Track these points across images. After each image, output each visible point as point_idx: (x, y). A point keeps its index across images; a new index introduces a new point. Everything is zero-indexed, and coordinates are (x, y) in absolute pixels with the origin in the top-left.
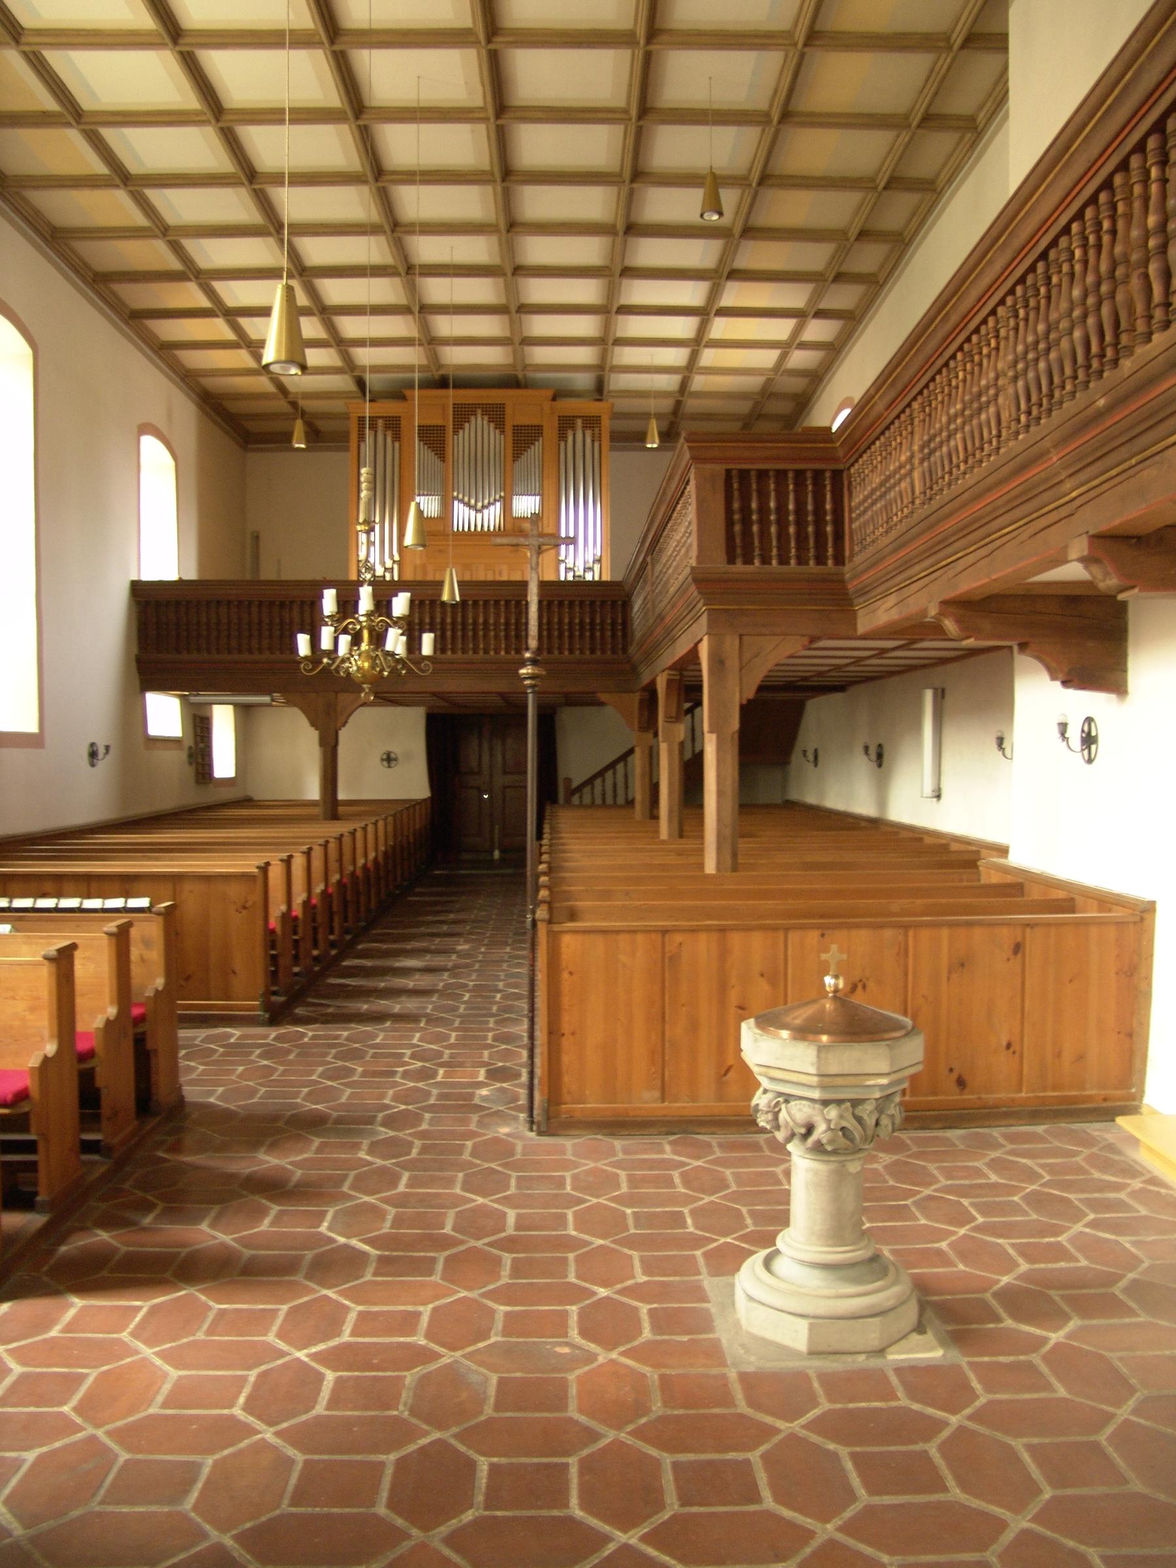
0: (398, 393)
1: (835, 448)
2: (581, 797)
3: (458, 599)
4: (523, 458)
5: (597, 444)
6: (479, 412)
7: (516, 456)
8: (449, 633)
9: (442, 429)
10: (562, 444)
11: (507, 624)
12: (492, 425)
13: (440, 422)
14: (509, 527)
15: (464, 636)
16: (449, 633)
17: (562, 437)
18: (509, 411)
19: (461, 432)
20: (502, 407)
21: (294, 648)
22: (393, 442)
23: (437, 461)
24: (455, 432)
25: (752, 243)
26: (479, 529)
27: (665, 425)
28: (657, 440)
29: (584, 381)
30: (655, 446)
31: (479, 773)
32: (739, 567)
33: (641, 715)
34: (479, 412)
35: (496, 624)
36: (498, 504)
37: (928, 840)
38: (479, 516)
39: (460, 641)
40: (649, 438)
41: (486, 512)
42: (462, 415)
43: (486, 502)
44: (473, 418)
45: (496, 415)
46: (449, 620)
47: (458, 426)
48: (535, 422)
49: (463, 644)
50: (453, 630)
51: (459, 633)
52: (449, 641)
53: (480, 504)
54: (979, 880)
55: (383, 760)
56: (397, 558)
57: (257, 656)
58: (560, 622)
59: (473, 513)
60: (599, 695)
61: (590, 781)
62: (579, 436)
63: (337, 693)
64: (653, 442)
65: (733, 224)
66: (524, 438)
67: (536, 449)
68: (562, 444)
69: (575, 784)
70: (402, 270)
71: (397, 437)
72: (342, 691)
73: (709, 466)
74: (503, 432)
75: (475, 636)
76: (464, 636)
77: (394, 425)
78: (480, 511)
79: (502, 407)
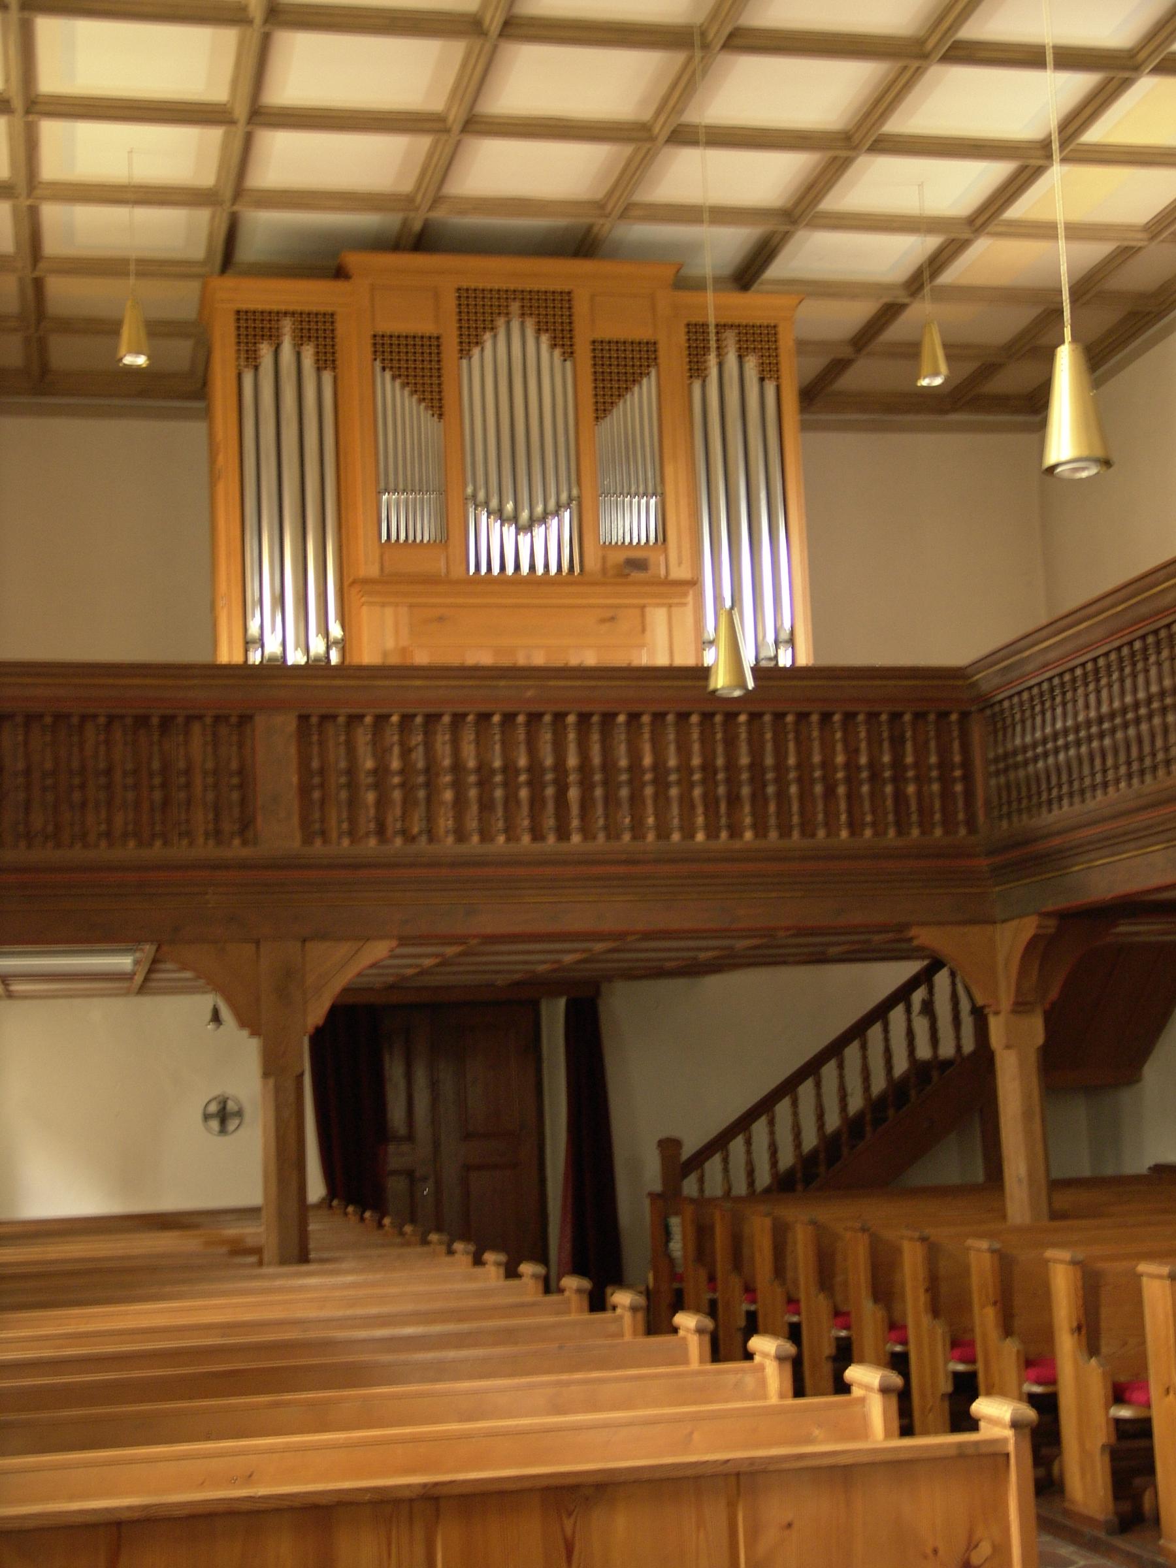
2: (701, 1180)
3: (751, 684)
4: (618, 412)
5: (770, 388)
6: (515, 307)
8: (573, 794)
9: (434, 343)
10: (697, 386)
11: (708, 768)
12: (545, 339)
13: (426, 327)
14: (592, 563)
15: (610, 800)
16: (573, 794)
17: (696, 369)
18: (581, 308)
19: (476, 351)
20: (565, 299)
22: (319, 370)
23: (427, 420)
24: (464, 352)
26: (525, 569)
27: (816, 364)
28: (943, 368)
31: (410, 1138)
33: (1023, 972)
35: (685, 768)
36: (567, 515)
38: (524, 540)
39: (600, 810)
40: (926, 364)
41: (539, 531)
43: (539, 509)
44: (501, 322)
47: (469, 340)
51: (599, 792)
52: (575, 810)
53: (525, 515)
55: (207, 1117)
56: (336, 631)
57: (103, 853)
59: (510, 531)
61: (720, 1143)
64: (936, 374)
65: (449, 109)
67: (645, 393)
68: (697, 386)
70: (18, 103)
71: (327, 360)
72: (322, 936)
74: (569, 354)
75: (636, 799)
76: (610, 800)
78: (529, 528)
79: (565, 299)
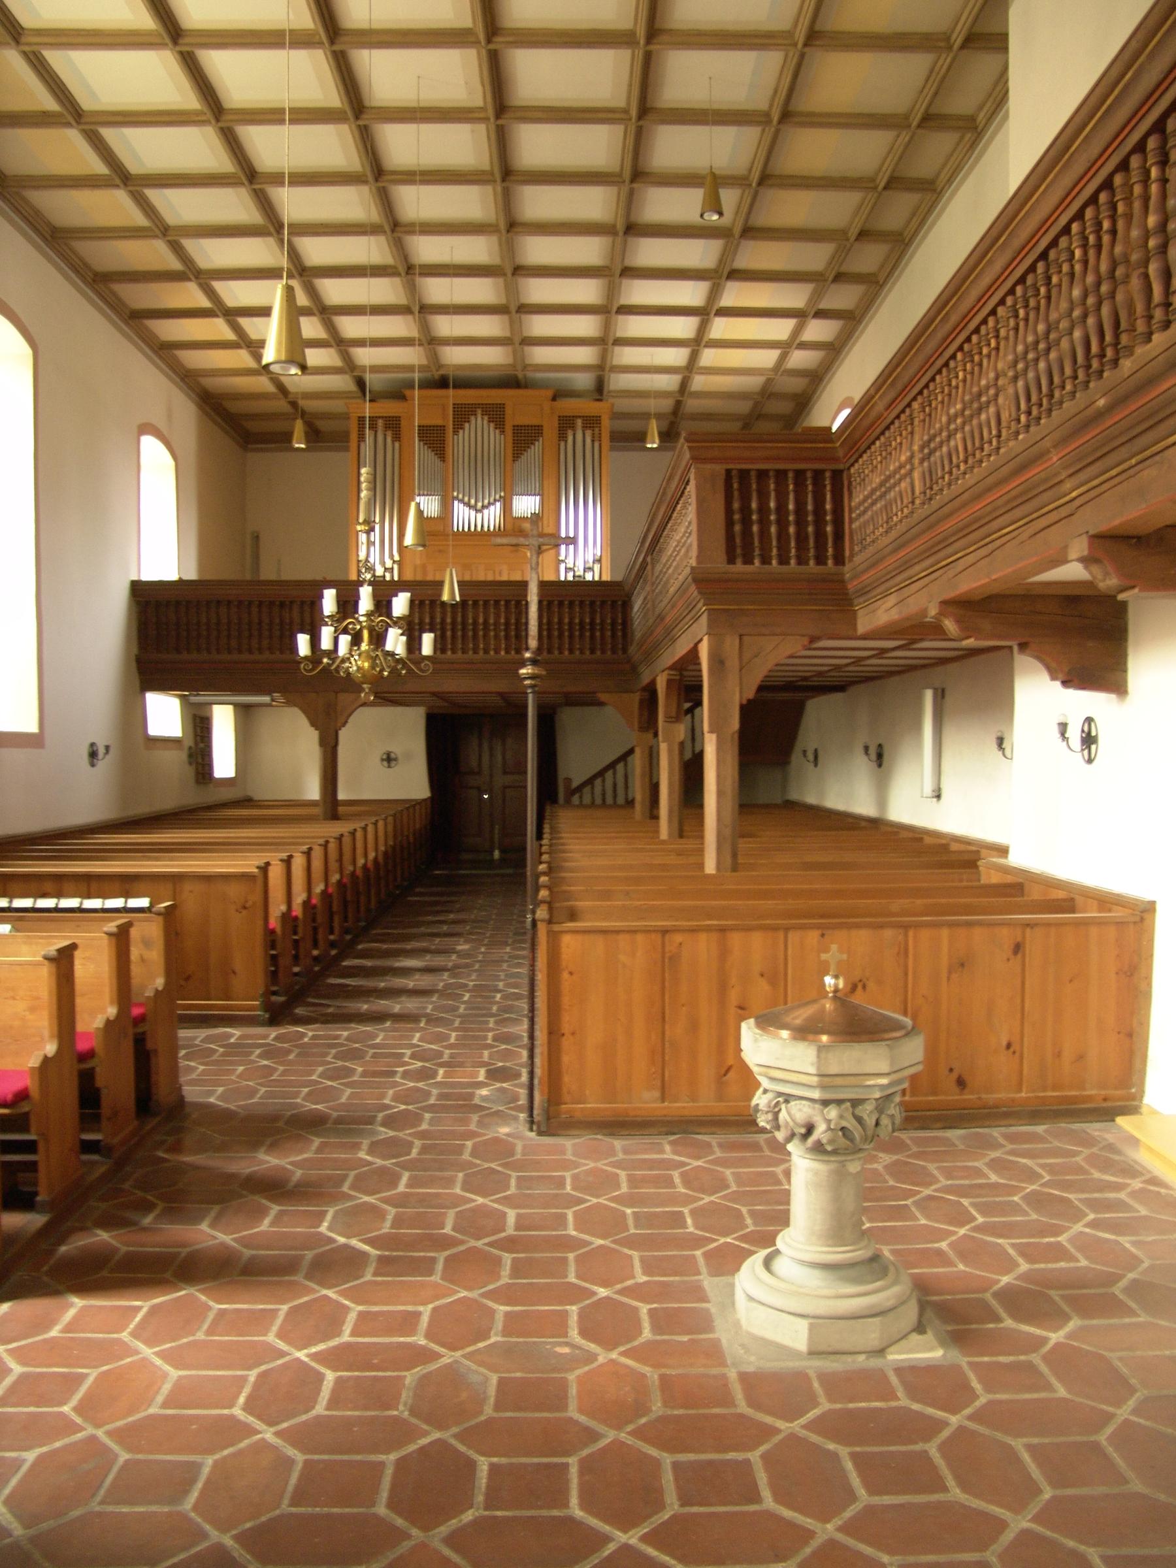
0: (398, 393)
1: (835, 448)
2: (581, 797)
3: (458, 599)
4: (523, 458)
5: (597, 444)
6: (479, 412)
7: (516, 456)
8: (449, 633)
9: (442, 429)
10: (562, 444)
11: (507, 624)
12: (492, 425)
13: (440, 422)
14: (509, 527)
15: (464, 636)
16: (449, 633)
17: (562, 437)
18: (509, 411)
19: (461, 432)
20: (502, 407)
21: (294, 648)
22: (393, 442)
23: (437, 461)
24: (455, 432)
25: (752, 243)
26: (479, 529)
27: (665, 425)
28: (657, 440)
29: (584, 381)
30: (655, 446)
31: (479, 773)
32: (739, 567)
33: (641, 715)
34: (479, 412)
35: (496, 624)
36: (498, 504)
37: (928, 840)
38: (479, 516)
39: (460, 641)
40: (649, 438)
41: (486, 512)
42: (462, 415)
43: (486, 502)
44: (473, 418)
45: (496, 415)
46: (449, 620)
47: (458, 426)
48: (535, 422)
49: (463, 644)
50: (453, 630)
51: (459, 633)
52: (449, 641)
53: (480, 504)
54: (979, 880)
55: (383, 760)
56: (397, 558)
57: (257, 656)
58: (560, 622)
59: (473, 513)
60: (599, 695)
61: (590, 781)
62: (579, 436)
63: (337, 693)
64: (653, 442)
66: (524, 438)
67: (536, 449)
68: (562, 444)
69: (575, 784)
70: (402, 270)
71: (397, 437)
72: (342, 691)
73: (709, 466)
74: (503, 432)
75: (475, 636)
76: (464, 636)
77: (394, 425)
78: (480, 511)
79: (502, 407)
